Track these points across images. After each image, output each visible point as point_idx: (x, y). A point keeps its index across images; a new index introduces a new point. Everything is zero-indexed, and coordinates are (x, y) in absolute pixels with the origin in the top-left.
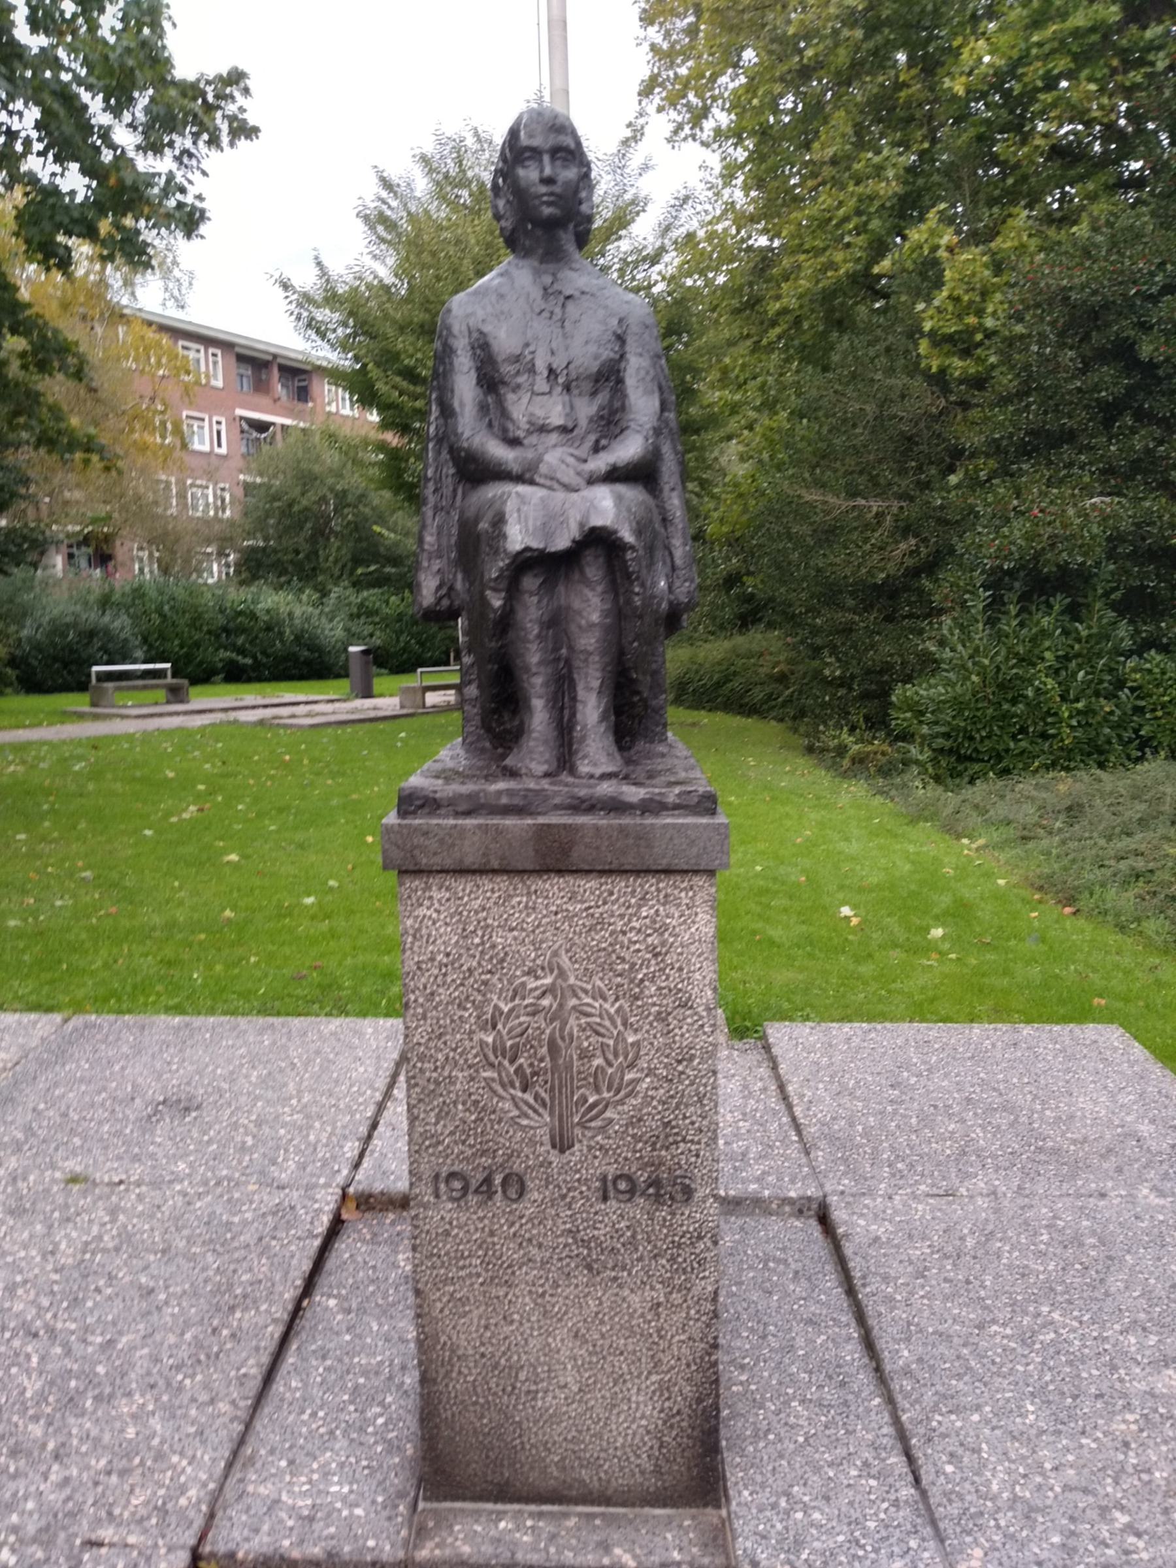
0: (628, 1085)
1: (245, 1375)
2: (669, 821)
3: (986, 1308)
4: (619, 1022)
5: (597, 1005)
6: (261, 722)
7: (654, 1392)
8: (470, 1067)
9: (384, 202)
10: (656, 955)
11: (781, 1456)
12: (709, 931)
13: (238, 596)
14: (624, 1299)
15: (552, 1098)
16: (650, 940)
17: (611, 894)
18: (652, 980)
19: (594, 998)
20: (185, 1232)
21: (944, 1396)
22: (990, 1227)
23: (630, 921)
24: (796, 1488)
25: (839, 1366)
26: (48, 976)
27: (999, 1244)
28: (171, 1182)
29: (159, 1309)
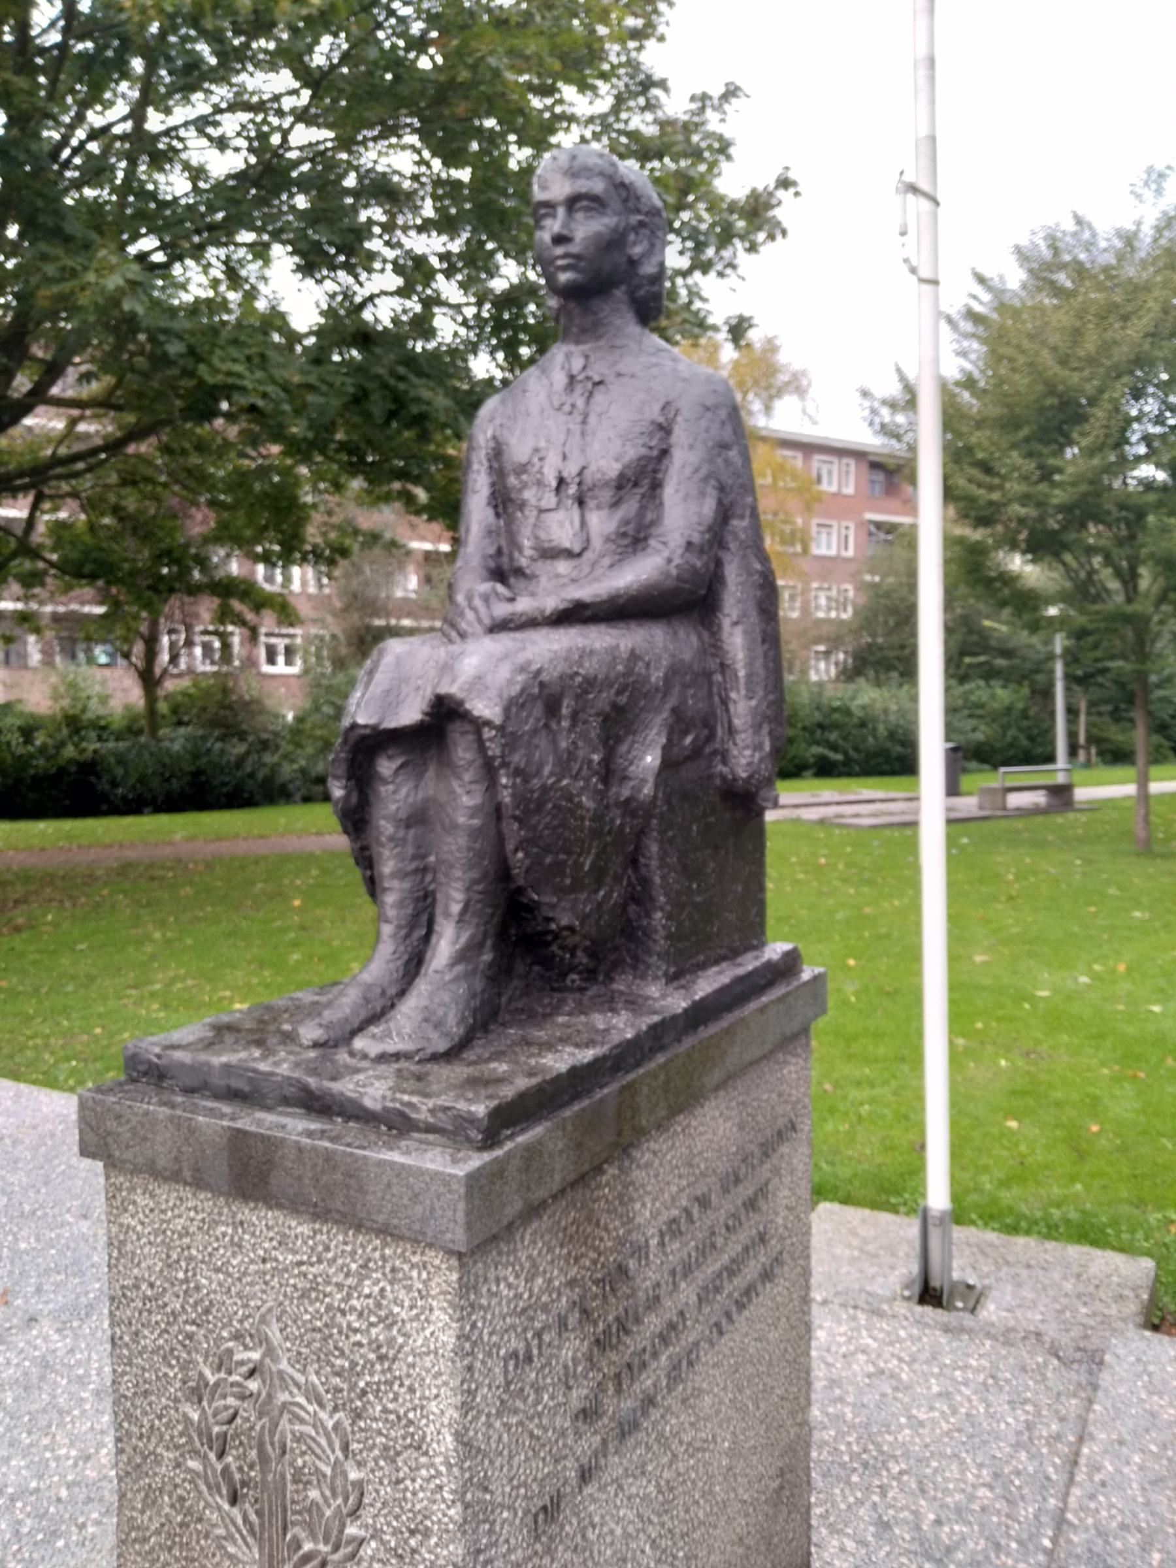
0: (349, 1543)
2: (396, 1157)
5: (311, 1409)
6: (822, 822)
9: (975, 297)
12: (448, 1339)
13: (836, 694)
16: (374, 1331)
17: (327, 1249)
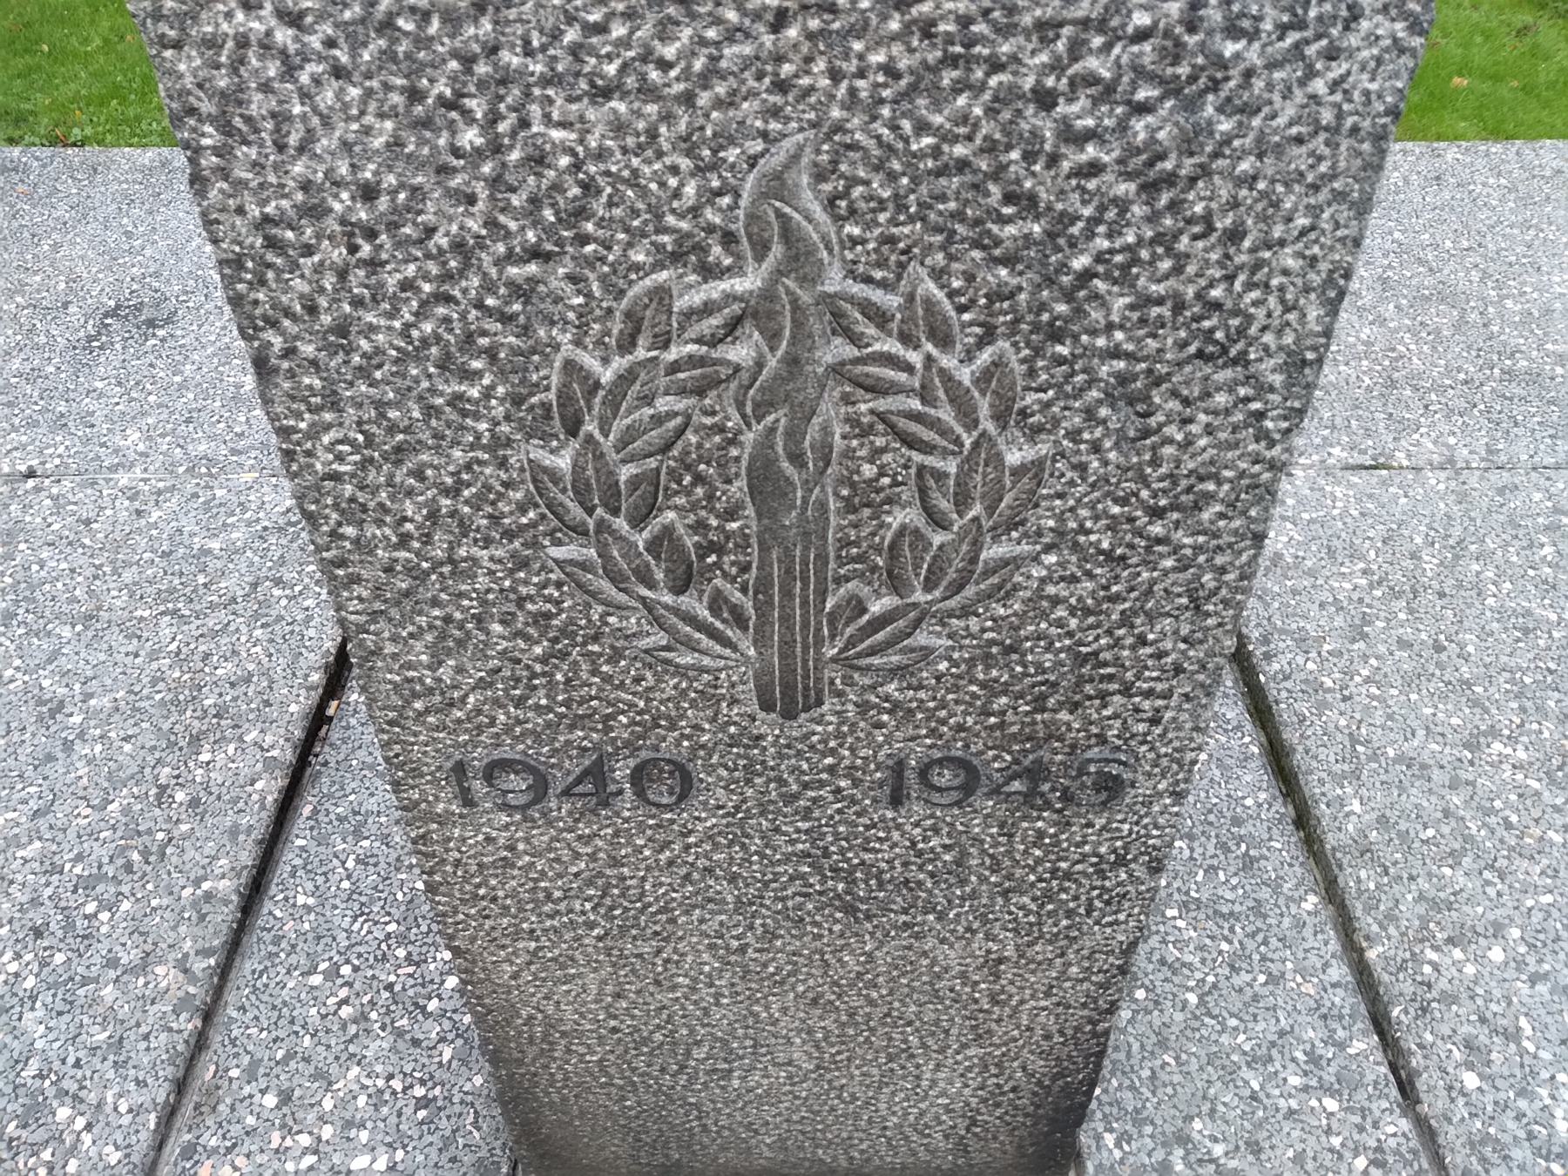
0: (987, 573)
1: (208, 896)
3: (1475, 703)
4: (984, 407)
5: (915, 358)
7: (969, 1069)
8: (509, 535)
10: (1150, 189)
11: (1163, 1044)
14: (925, 954)
15: (763, 609)
16: (1140, 126)
18: (1124, 278)
19: (906, 339)
20: (128, 576)
21: (1435, 905)
22: (1457, 532)
23: (1077, 50)
24: (1197, 1124)
25: (1237, 822)
26: (20, 63)
27: (1476, 567)
28: (113, 469)
29: (68, 746)
